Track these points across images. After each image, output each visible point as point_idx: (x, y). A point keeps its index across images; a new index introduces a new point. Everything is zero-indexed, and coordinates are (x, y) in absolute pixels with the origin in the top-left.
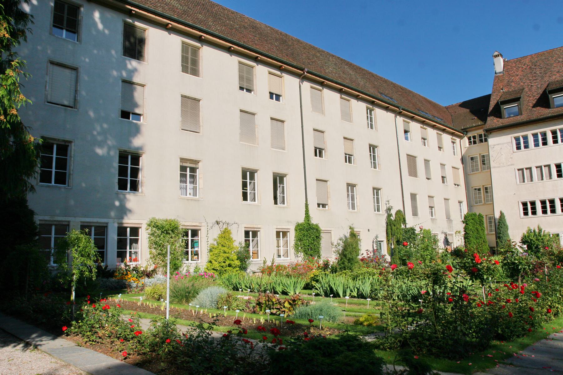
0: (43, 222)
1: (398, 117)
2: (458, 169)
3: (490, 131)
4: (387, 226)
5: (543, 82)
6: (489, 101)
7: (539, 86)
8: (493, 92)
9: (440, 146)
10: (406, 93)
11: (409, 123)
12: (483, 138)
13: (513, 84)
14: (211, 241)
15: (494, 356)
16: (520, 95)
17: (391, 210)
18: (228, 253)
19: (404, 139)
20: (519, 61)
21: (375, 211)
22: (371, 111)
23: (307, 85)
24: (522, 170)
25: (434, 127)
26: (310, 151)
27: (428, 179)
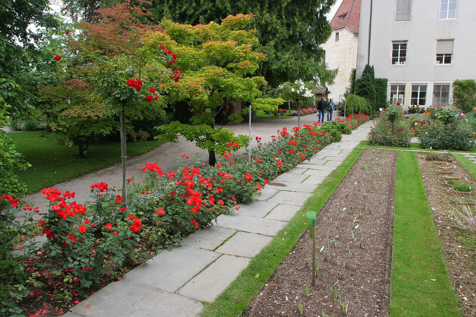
0: (393, 85)
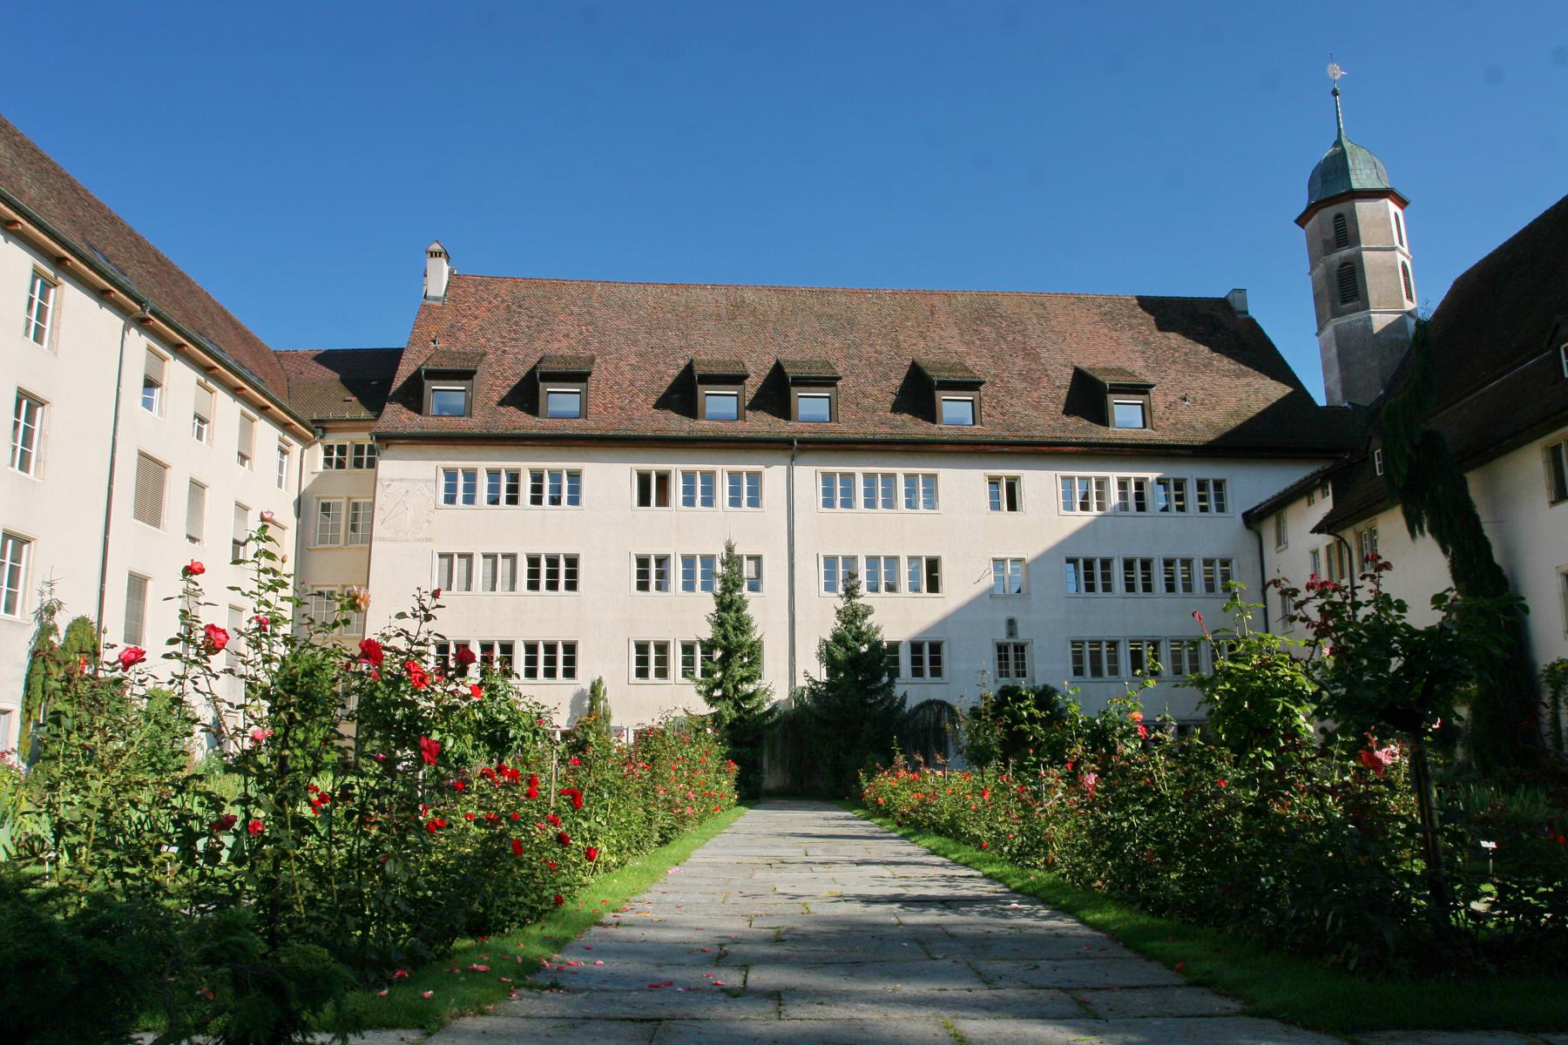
1: (134, 331)
2: (283, 528)
3: (387, 440)
4: (32, 662)
5: (530, 351)
6: (398, 363)
7: (520, 357)
8: (412, 343)
9: (244, 453)
10: (169, 274)
11: (164, 359)
12: (365, 456)
13: (462, 336)
15: (492, 968)
16: (476, 367)
17: (57, 614)
19: (140, 402)
20: (485, 283)
22: (48, 285)
24: (450, 556)
25: (236, 392)
27: (193, 539)
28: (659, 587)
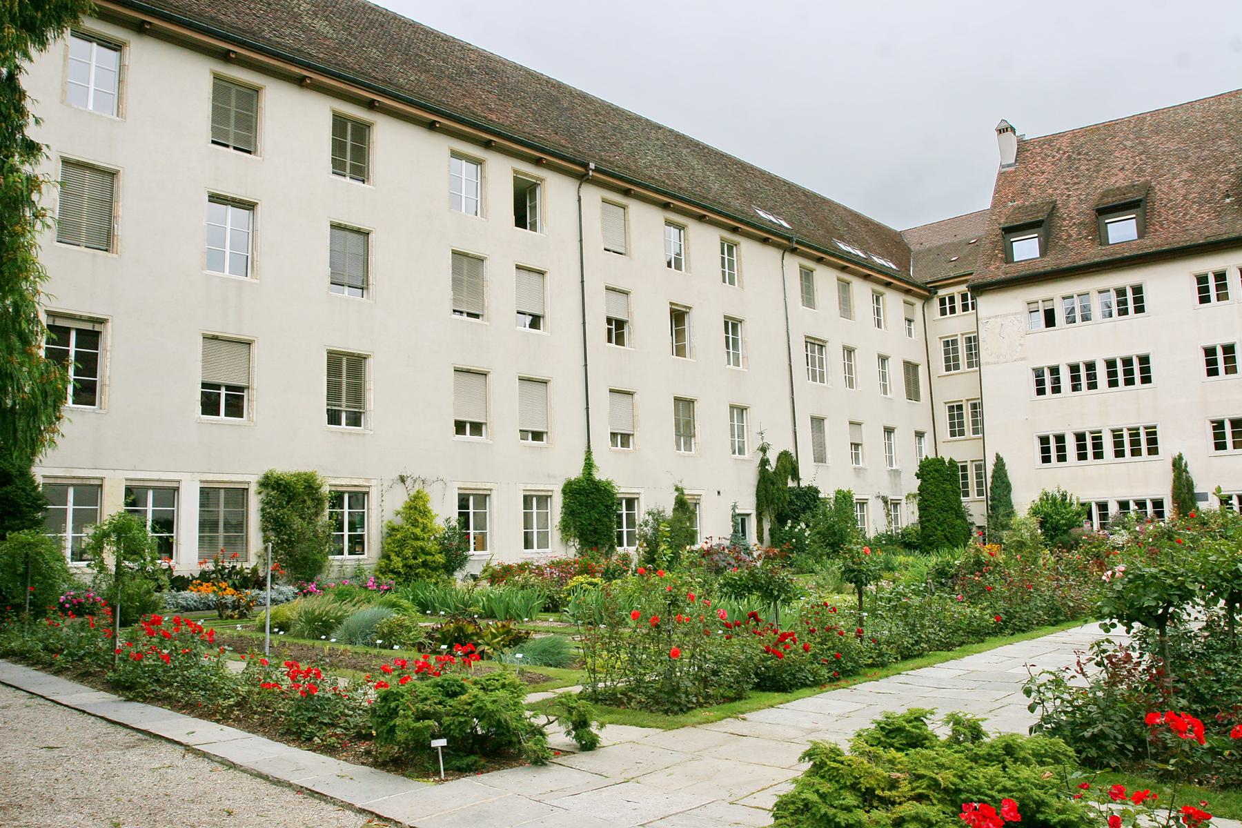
0: (52, 481)
7: (1082, 197)
13: (1033, 191)
14: (389, 516)
18: (423, 539)
21: (734, 453)
22: (730, 249)
23: (593, 196)
26: (598, 329)
28: (1100, 432)
